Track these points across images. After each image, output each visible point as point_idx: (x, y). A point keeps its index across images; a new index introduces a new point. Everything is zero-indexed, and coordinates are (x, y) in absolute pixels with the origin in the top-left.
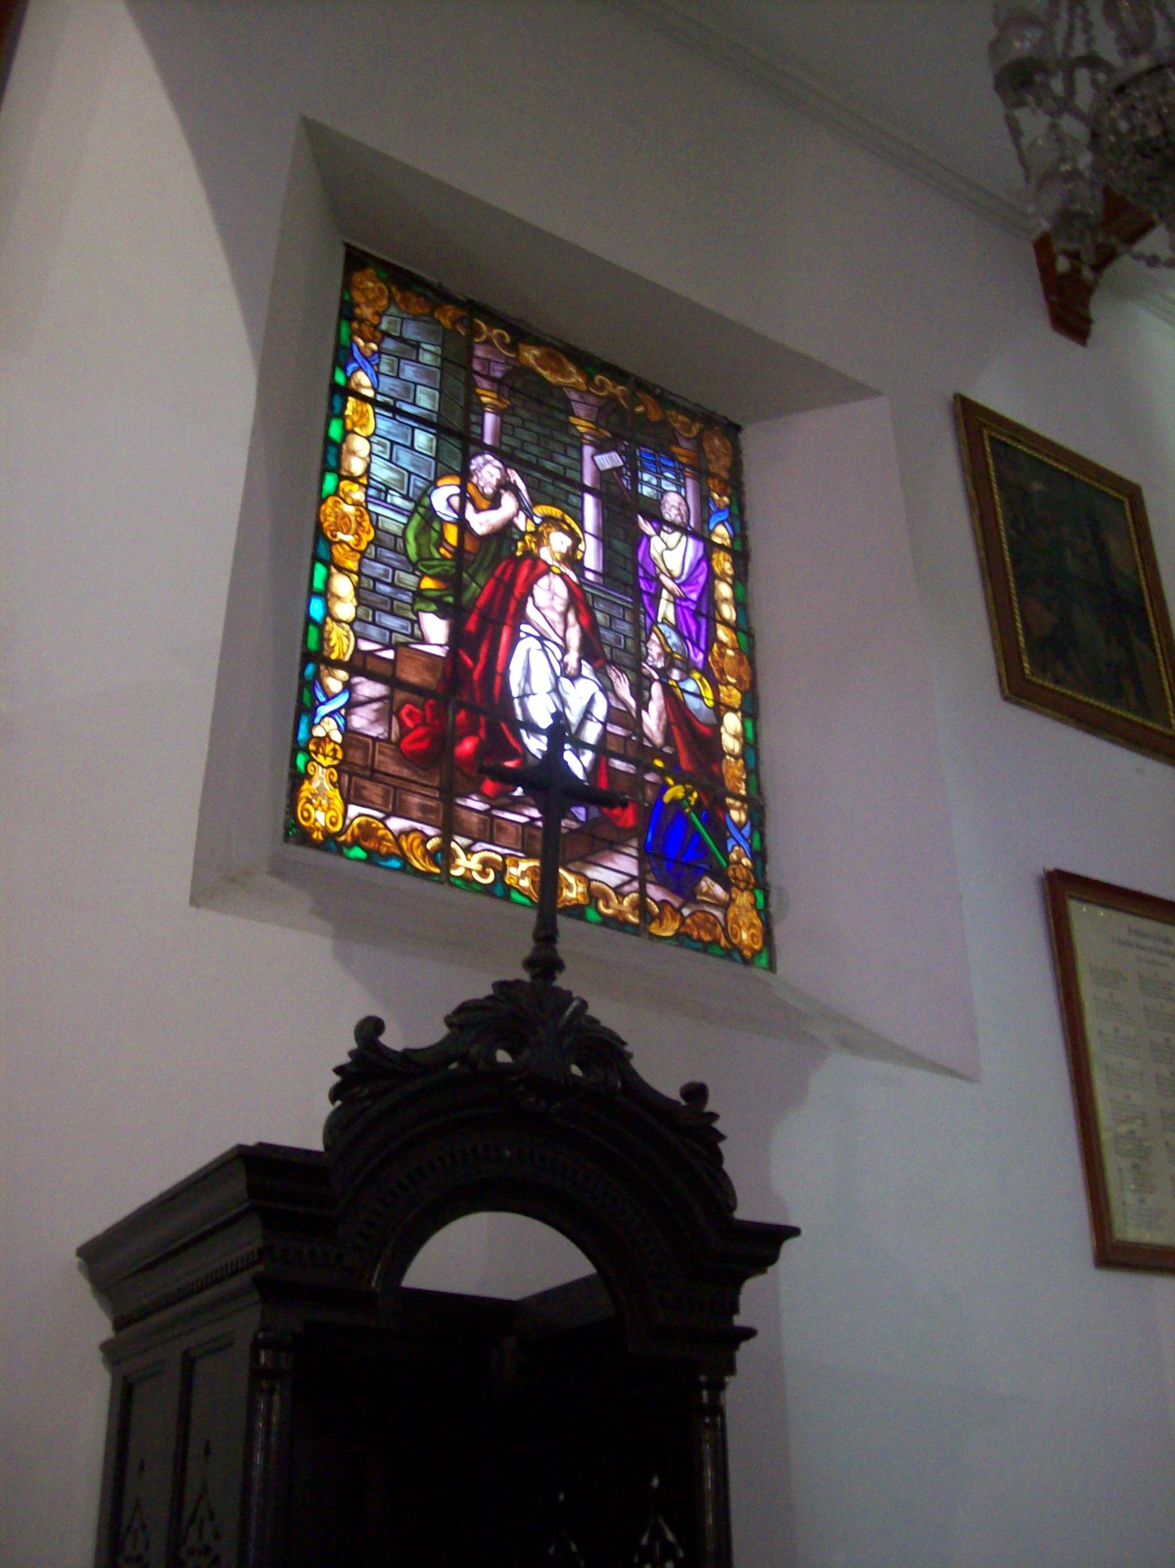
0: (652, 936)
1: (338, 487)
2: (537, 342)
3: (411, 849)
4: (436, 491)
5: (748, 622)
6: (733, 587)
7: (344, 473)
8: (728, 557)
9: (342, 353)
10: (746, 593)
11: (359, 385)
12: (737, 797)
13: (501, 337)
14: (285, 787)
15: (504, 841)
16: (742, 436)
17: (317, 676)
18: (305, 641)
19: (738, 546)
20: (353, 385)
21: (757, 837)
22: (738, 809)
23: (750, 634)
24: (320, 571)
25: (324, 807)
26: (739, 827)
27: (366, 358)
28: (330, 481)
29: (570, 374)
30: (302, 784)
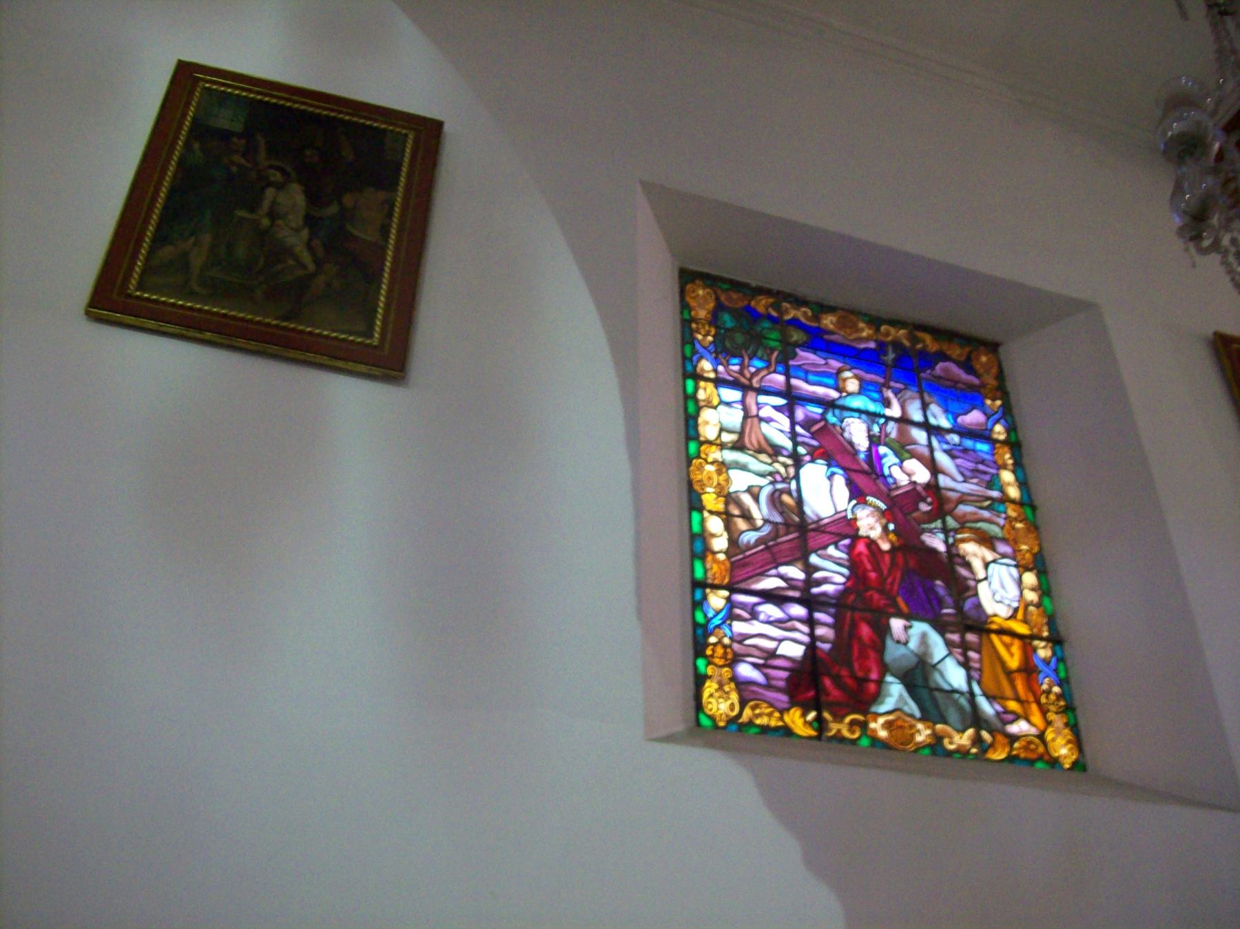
0: (989, 760)
1: (699, 452)
2: (832, 309)
3: (793, 722)
4: (823, 515)
5: (1029, 496)
6: (1014, 472)
7: (702, 439)
8: (1006, 449)
9: (700, 632)
10: (1025, 474)
11: (703, 370)
12: (1042, 639)
13: (805, 313)
14: (692, 686)
15: (787, 546)
16: (1001, 350)
17: (705, 597)
18: (690, 526)
19: (1013, 438)
20: (698, 370)
21: (1061, 667)
22: (1044, 647)
23: (1034, 508)
24: (690, 384)
25: (720, 705)
26: (1046, 662)
27: (705, 348)
28: (693, 447)
29: (862, 330)
30: (704, 683)
